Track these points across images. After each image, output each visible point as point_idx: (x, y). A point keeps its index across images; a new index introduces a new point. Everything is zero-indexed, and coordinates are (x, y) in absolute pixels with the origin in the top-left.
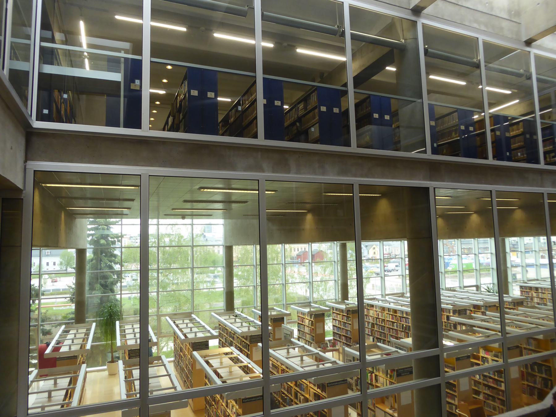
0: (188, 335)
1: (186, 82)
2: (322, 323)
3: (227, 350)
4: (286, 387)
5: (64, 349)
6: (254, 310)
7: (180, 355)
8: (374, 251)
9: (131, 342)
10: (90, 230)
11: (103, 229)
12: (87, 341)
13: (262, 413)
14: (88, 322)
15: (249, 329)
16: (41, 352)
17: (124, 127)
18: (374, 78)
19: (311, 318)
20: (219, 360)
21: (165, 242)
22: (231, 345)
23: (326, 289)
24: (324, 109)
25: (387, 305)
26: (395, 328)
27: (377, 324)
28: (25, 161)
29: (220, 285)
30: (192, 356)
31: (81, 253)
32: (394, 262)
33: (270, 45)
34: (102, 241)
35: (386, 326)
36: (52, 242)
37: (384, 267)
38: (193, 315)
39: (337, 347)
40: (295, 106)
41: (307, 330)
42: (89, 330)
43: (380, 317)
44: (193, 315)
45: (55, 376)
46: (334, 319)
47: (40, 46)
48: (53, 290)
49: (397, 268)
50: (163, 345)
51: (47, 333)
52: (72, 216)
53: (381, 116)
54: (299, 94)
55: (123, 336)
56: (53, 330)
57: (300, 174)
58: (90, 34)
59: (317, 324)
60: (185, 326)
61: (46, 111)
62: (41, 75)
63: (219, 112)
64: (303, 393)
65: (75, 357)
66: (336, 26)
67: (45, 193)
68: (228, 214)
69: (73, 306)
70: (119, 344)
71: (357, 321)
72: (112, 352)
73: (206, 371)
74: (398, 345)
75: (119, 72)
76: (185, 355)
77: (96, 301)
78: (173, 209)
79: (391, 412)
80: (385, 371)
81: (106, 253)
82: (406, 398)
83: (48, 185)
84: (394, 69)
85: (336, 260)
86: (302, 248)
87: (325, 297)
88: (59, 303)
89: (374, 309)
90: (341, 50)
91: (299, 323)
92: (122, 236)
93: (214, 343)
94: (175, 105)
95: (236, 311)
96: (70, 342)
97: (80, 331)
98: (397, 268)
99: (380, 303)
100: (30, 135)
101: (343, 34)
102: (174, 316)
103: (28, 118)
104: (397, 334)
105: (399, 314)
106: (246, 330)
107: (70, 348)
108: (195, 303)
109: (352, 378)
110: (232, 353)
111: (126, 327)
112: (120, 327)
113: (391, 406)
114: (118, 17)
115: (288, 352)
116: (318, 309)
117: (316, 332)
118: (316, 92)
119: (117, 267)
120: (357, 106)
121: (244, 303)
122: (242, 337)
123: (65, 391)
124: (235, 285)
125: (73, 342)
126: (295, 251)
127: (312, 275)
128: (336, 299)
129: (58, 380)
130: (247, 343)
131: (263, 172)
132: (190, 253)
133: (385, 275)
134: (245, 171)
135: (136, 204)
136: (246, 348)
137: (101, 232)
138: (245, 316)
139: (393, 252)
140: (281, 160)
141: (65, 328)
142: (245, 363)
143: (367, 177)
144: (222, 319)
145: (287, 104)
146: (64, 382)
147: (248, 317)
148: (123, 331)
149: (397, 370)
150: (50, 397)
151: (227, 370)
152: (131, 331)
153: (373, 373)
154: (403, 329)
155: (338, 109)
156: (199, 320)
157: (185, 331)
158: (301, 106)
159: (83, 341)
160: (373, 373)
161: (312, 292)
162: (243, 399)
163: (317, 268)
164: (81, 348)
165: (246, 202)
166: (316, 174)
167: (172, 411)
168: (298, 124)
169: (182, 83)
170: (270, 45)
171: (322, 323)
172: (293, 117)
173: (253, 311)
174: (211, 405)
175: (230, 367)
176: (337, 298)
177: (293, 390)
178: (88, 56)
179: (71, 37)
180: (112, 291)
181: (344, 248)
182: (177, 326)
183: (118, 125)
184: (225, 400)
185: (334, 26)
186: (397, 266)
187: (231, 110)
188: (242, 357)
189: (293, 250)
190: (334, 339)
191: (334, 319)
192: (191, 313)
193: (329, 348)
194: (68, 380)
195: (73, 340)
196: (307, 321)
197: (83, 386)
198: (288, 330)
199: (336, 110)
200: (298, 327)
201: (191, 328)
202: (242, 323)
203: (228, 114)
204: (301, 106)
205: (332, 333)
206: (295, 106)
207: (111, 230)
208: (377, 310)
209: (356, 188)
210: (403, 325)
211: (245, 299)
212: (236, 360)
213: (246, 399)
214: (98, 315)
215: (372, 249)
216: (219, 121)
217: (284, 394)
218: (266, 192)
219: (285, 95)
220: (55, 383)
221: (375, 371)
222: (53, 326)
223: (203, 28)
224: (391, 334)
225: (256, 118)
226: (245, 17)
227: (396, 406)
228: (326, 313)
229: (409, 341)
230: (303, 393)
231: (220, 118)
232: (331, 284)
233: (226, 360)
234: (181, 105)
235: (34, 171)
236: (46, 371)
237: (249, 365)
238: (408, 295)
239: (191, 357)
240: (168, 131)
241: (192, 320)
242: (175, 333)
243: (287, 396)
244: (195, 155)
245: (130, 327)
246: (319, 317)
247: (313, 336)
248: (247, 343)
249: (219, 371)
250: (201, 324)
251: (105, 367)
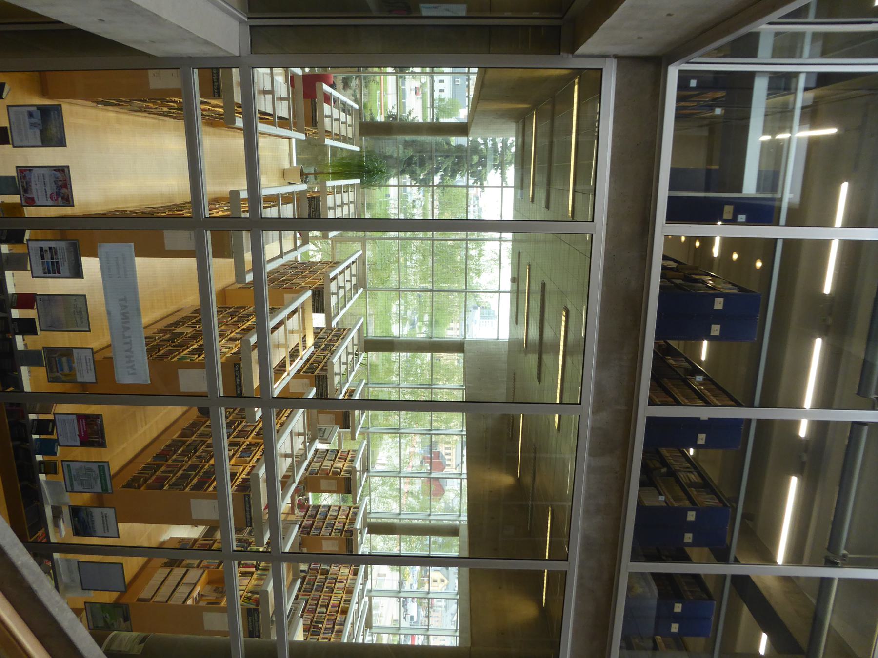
0: (334, 282)
1: (735, 291)
2: (334, 489)
3: (310, 341)
4: (248, 429)
5: (326, 107)
6: (364, 382)
7: (305, 269)
8: (439, 581)
9: (330, 201)
10: (493, 140)
11: (495, 160)
12: (336, 140)
13: (222, 394)
14: (361, 139)
15: (336, 374)
16: (323, 78)
17: (669, 197)
18: (745, 610)
19: (346, 471)
20: (296, 328)
21: (472, 249)
22: (316, 345)
23: (385, 497)
24: (691, 516)
25: (355, 599)
26: (318, 610)
27: (326, 579)
28: (616, 56)
29: (397, 331)
30: (303, 289)
31: (461, 129)
32: (418, 613)
33: (803, 431)
34: (475, 159)
35: (323, 594)
36: (484, 94)
37: (413, 598)
38: (362, 289)
39: (297, 511)
40: (695, 468)
41: (327, 464)
42: (350, 141)
43: (337, 585)
44: (362, 289)
45: (292, 98)
46: (340, 508)
47: (800, 72)
48: (404, 90)
49: (408, 617)
50: (319, 244)
51: (346, 84)
52: (521, 119)
53: (676, 618)
54: (713, 474)
55: (340, 190)
56: (349, 92)
57: (588, 473)
58: (813, 143)
59: (334, 481)
60: (348, 278)
61: (693, 83)
62: (751, 75)
63: (682, 342)
64: (238, 454)
65: (314, 123)
66: (845, 552)
67: (565, 83)
68: (514, 345)
69: (380, 118)
70: (330, 183)
71: (334, 550)
72: (316, 174)
73: (284, 309)
74: (294, 614)
75: (758, 189)
76: (304, 278)
77: (389, 150)
78: (530, 266)
79: (195, 594)
80: (259, 589)
81: (457, 163)
82: (215, 621)
83: (576, 87)
84: (762, 650)
85: (432, 517)
86: (449, 460)
87: (373, 495)
88: (386, 98)
89: (351, 577)
90: (796, 556)
91: (338, 451)
92: (482, 186)
93: (319, 320)
94: (695, 272)
95: (364, 355)
96: (336, 116)
97: (349, 129)
98: (408, 617)
99: (359, 587)
100: (654, 64)
101: (833, 564)
102: (362, 262)
103: (685, 59)
104: (309, 612)
105: (339, 617)
106: (336, 369)
107: (327, 117)
108: (379, 293)
109: (250, 533)
110: (305, 347)
111: (351, 194)
112: (352, 185)
113: (202, 595)
114: (845, 187)
115: (299, 434)
116: (358, 485)
117: (323, 478)
118: (721, 505)
119: (437, 179)
120: (696, 577)
121: (374, 367)
122: (326, 363)
123: (271, 112)
124: (403, 354)
125: (335, 120)
126: (446, 448)
127: (411, 477)
128: (370, 513)
129: (286, 102)
130: (317, 373)
131: (593, 413)
132: (455, 286)
133: (400, 598)
134: (596, 383)
135: (538, 212)
136: (308, 369)
137: (491, 156)
138: (356, 369)
139: (435, 614)
140: (613, 442)
141: (355, 109)
142: (289, 368)
143: (578, 587)
144: (354, 333)
145: (696, 453)
146: (283, 110)
147: (353, 373)
148: (346, 189)
149: (257, 610)
150: (265, 92)
151: (282, 341)
152: (345, 201)
153: (257, 569)
154: (316, 622)
155: (690, 541)
156: (354, 298)
157: (341, 278)
158: (694, 477)
159: (336, 134)
160: (257, 569)
161: (384, 475)
162: (239, 364)
163: (418, 485)
164: (327, 131)
165: (539, 380)
166: (586, 498)
167: (232, 260)
168: (664, 470)
169: (733, 285)
170: (803, 431)
171: (334, 489)
172: (677, 464)
173: (361, 380)
174: (232, 315)
175: (286, 345)
176: (372, 515)
177: (243, 440)
178: (780, 143)
179: (812, 115)
180: (403, 172)
181: (453, 531)
182: (347, 267)
183: (672, 187)
184: (239, 336)
185: (846, 549)
186: (412, 618)
187: (687, 360)
188: (298, 364)
189: (447, 446)
190: (309, 507)
191: (340, 508)
192: (365, 287)
193: (297, 498)
194: (286, 115)
195: (338, 120)
196: (340, 465)
197: (270, 135)
198: (331, 434)
199: (688, 538)
200: (333, 451)
201: (344, 287)
202: (346, 363)
203: (681, 355)
204: (694, 477)
205: (317, 503)
206: (695, 468)
207: (493, 171)
208: (349, 581)
209: (559, 566)
210: (322, 623)
211: (380, 367)
212: (294, 354)
213: (239, 369)
214: (370, 153)
215: (446, 583)
216: (670, 342)
217: (238, 425)
218: (557, 416)
219: (711, 452)
220: (282, 99)
221: (259, 572)
222: (354, 91)
223: (830, 321)
224: (310, 602)
225: (678, 404)
226: (858, 394)
227: (202, 604)
228: (350, 496)
229: (299, 636)
230: (238, 454)
231: (673, 343)
232: (395, 508)
233: (296, 339)
234: (697, 281)
235: (602, 69)
236: (299, 84)
237: (286, 374)
238: (368, 640)
239: (303, 287)
240: (663, 266)
241: (355, 288)
242: (338, 263)
243: (235, 429)
244: (623, 306)
245: (351, 199)
246: (346, 485)
247: (316, 474)
248: (317, 373)
249: (282, 328)
250: (348, 301)
251: (295, 164)
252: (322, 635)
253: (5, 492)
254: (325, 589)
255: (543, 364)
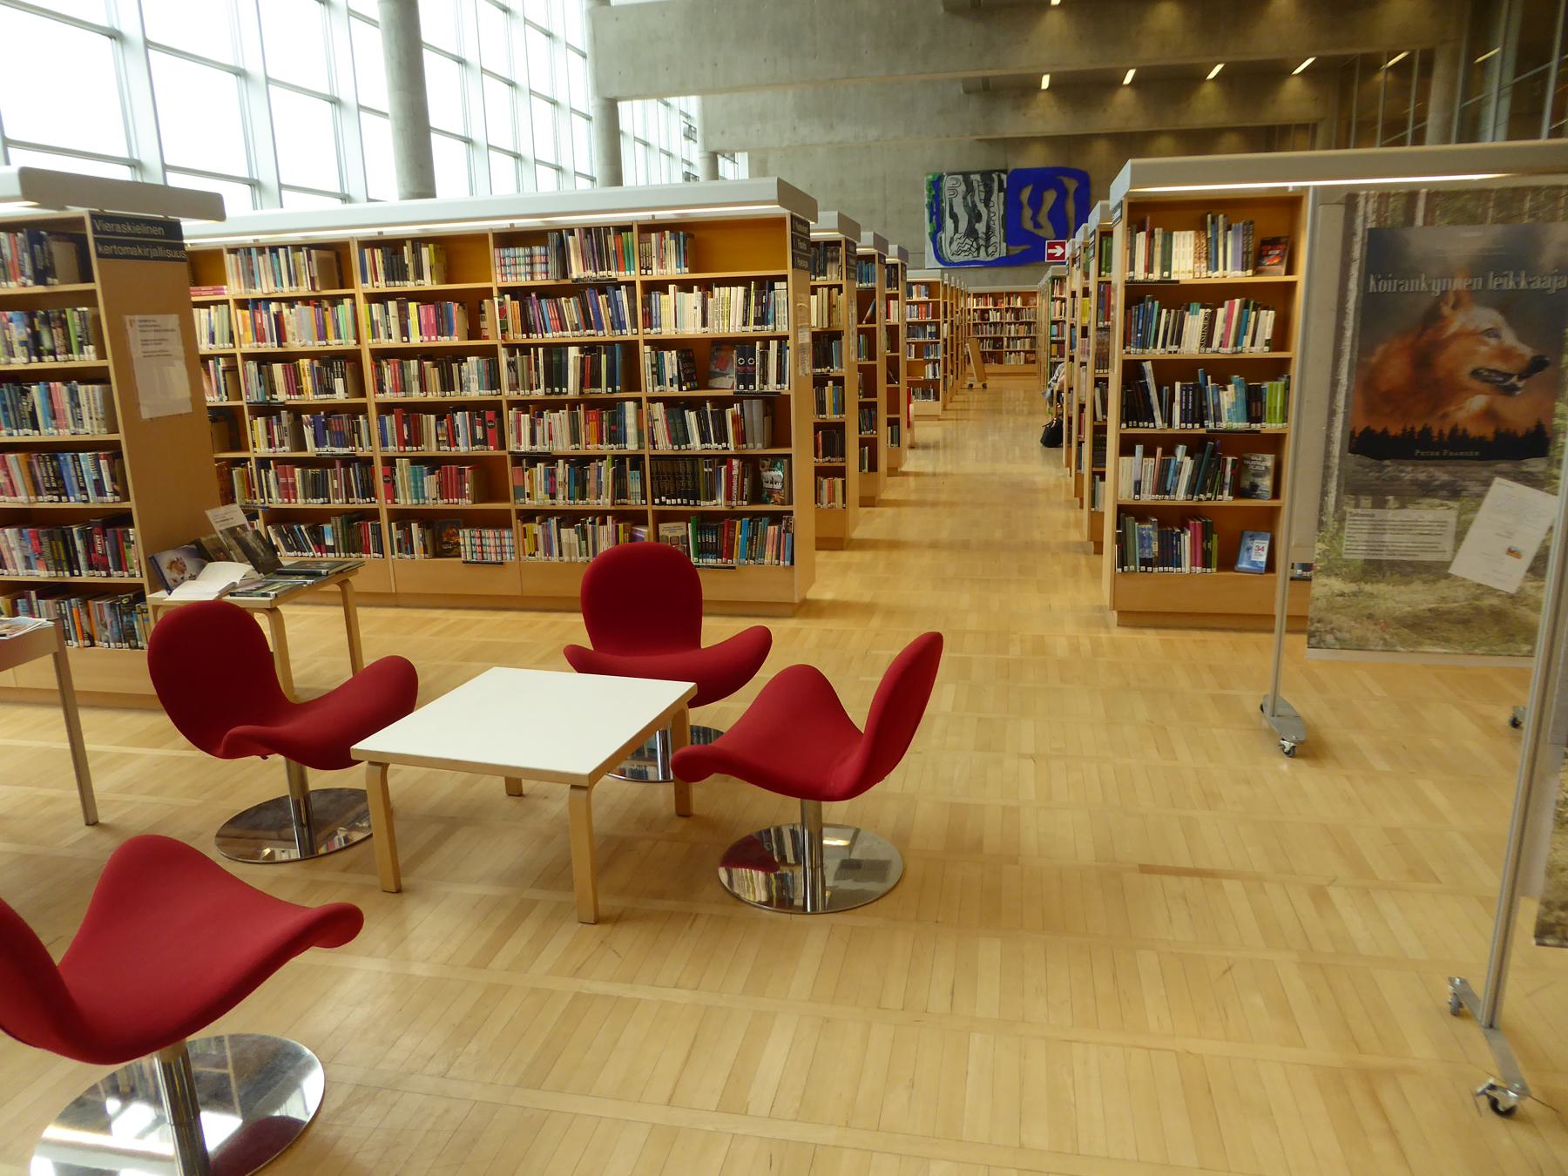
27: (267, 410)
89: (234, 289)
208: (264, 288)
252: (628, 334)
253: (250, 992)
254: (340, 395)
255: (1334, 306)
